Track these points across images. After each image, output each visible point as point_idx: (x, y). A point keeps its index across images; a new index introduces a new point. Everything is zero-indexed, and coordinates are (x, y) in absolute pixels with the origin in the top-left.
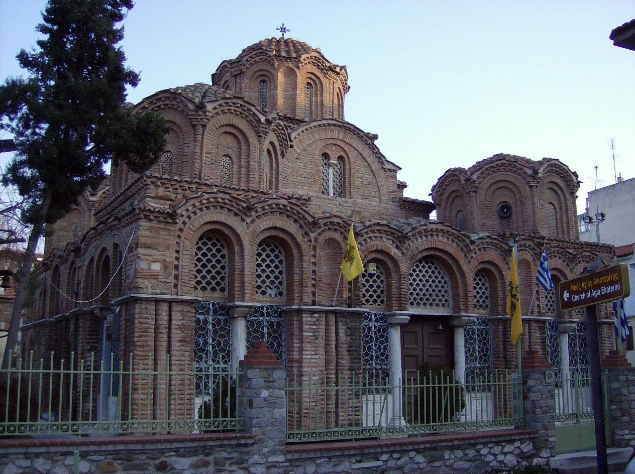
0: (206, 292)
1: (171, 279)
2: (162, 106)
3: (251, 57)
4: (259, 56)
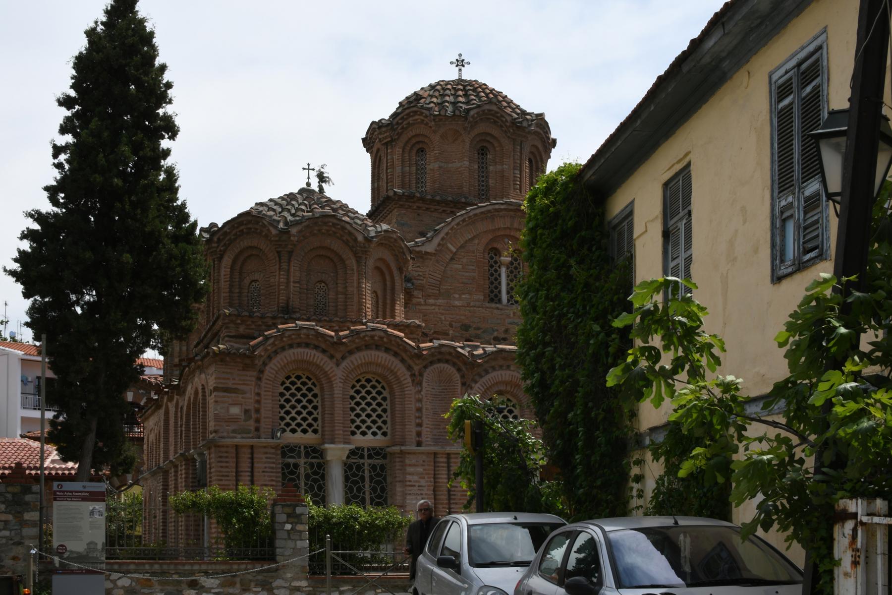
0: (296, 434)
1: (251, 424)
3: (402, 118)
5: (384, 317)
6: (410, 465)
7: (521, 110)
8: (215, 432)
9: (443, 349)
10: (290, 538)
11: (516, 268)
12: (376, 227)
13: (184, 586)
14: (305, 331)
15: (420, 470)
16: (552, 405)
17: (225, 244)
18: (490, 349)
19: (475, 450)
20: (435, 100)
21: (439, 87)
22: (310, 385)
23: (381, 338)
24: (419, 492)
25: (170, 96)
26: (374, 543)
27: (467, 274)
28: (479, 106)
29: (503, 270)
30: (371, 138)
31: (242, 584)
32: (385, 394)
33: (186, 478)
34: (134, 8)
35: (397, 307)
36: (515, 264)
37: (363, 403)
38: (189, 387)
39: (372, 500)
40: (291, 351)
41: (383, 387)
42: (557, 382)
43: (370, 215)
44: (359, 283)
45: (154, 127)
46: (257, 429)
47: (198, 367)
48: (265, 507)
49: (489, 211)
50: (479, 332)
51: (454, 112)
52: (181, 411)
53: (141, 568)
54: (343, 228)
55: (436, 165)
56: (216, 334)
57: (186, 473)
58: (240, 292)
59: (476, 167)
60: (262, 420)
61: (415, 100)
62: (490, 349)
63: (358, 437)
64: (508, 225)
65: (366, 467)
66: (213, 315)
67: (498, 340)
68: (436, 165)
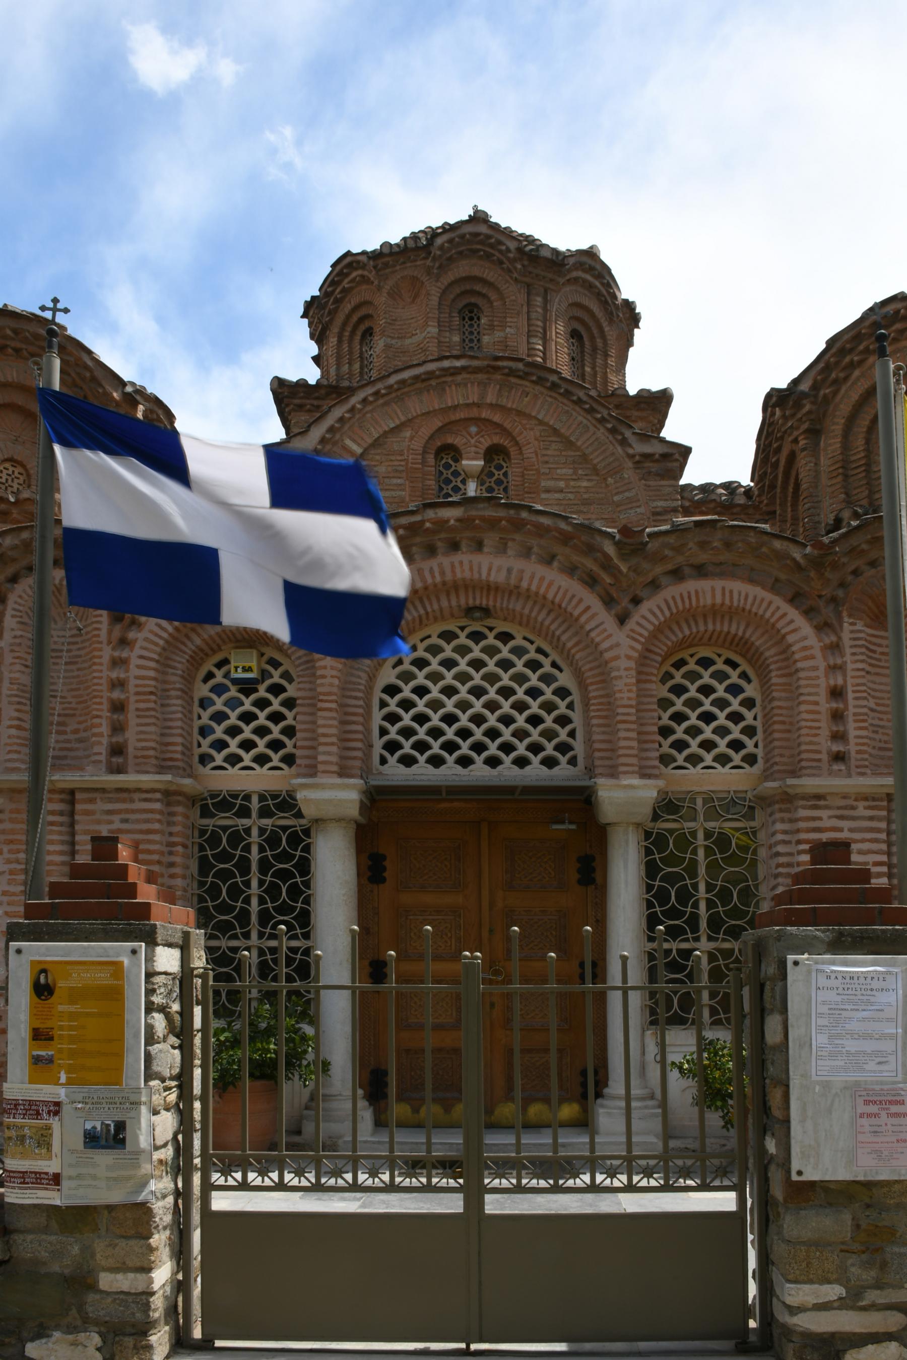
64: (474, 398)
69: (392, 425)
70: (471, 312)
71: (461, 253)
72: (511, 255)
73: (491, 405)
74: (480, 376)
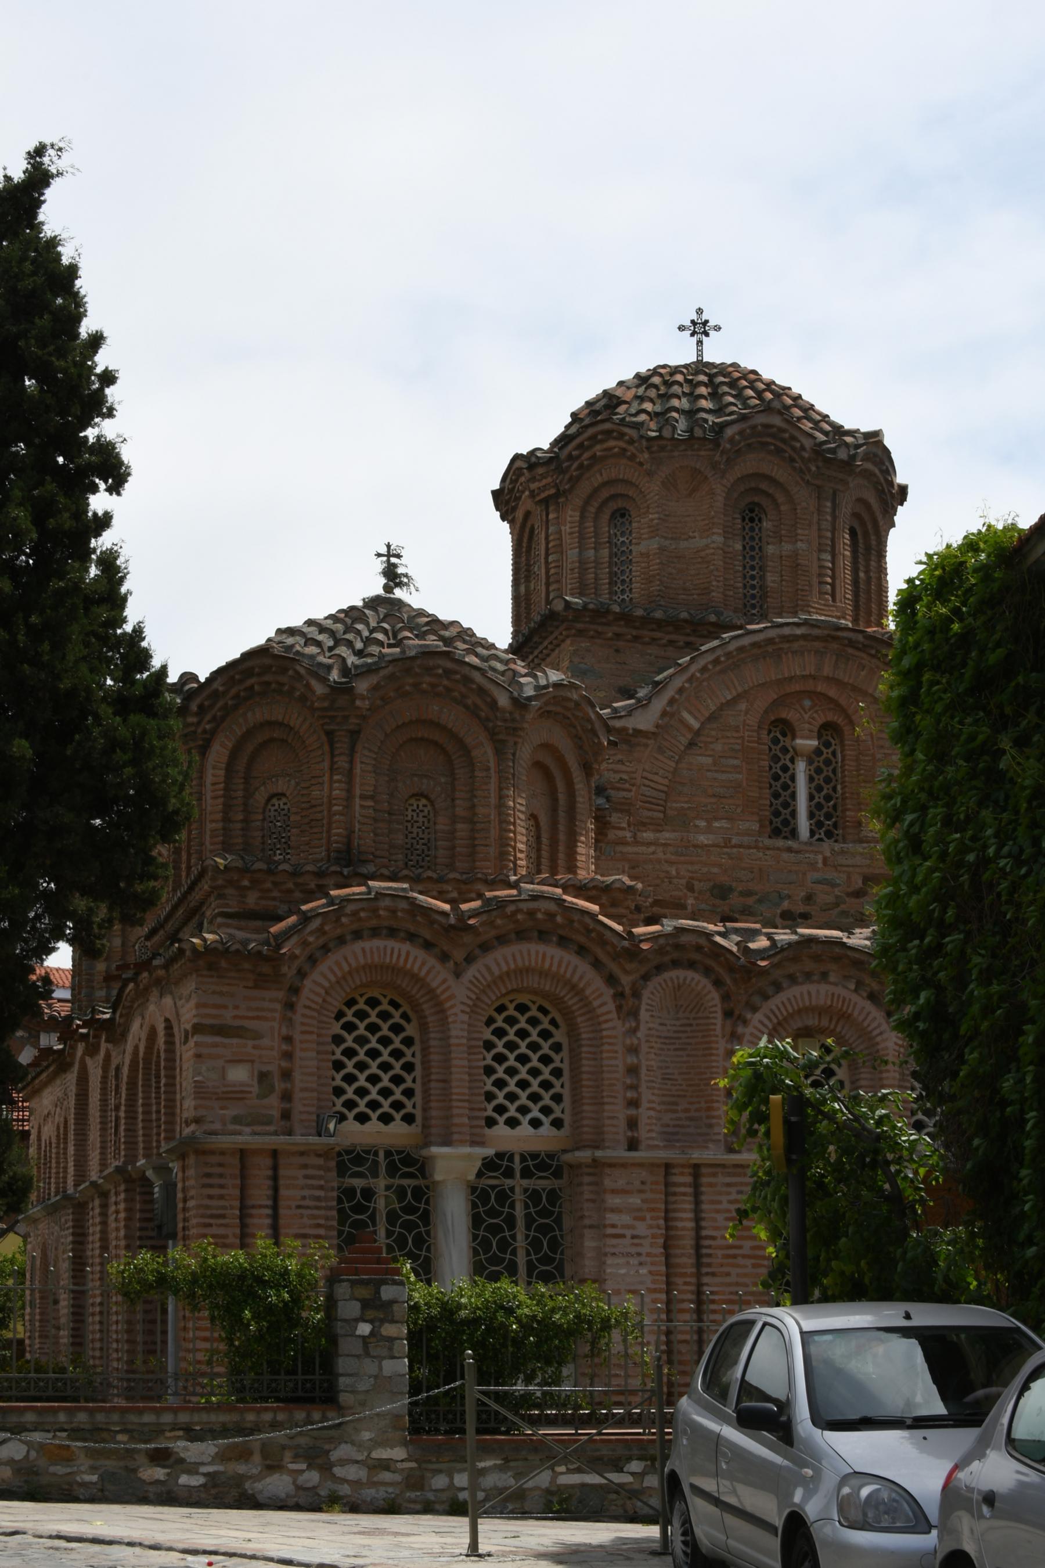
0: (368, 1125)
1: (274, 1102)
2: (256, 687)
3: (580, 446)
4: (601, 441)
5: (554, 871)
6: (613, 1191)
7: (832, 424)
8: (197, 1121)
9: (684, 939)
10: (367, 1354)
11: (828, 763)
12: (535, 677)
13: (142, 1459)
14: (387, 902)
15: (635, 1200)
16: (961, 1059)
17: (214, 718)
18: (784, 936)
19: (789, 1162)
20: (648, 406)
21: (656, 380)
22: (397, 1018)
23: (551, 916)
24: (633, 1250)
25: (110, 399)
26: (548, 1362)
27: (724, 777)
28: (743, 418)
29: (801, 769)
30: (511, 491)
31: (265, 1454)
32: (559, 1036)
33: (128, 1219)
34: (35, 215)
35: (581, 849)
36: (827, 753)
37: (512, 1057)
38: (135, 1026)
39: (531, 1267)
40: (358, 946)
41: (553, 1022)
42: (975, 1009)
43: (516, 648)
44: (501, 797)
45: (78, 468)
46: (286, 1115)
47: (158, 982)
48: (313, 1285)
49: (770, 641)
50: (750, 901)
51: (690, 430)
52: (117, 1077)
53: (50, 1419)
54: (467, 680)
55: (654, 545)
56: (195, 911)
57: (126, 1210)
58: (245, 820)
59: (739, 547)
60: (298, 1095)
61: (606, 407)
62: (784, 936)
63: (501, 1130)
65: (519, 1196)
66: (189, 868)
67: (790, 919)
68: (654, 545)
69: (729, 697)
70: (752, 511)
71: (749, 445)
72: (806, 455)
73: (828, 679)
74: (816, 644)
